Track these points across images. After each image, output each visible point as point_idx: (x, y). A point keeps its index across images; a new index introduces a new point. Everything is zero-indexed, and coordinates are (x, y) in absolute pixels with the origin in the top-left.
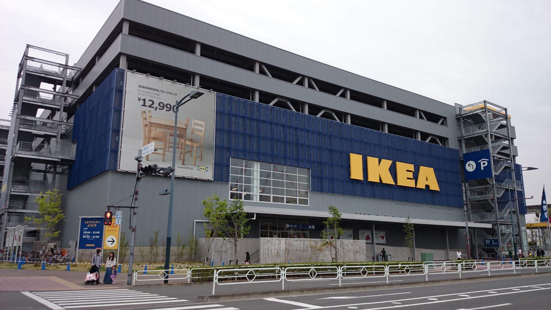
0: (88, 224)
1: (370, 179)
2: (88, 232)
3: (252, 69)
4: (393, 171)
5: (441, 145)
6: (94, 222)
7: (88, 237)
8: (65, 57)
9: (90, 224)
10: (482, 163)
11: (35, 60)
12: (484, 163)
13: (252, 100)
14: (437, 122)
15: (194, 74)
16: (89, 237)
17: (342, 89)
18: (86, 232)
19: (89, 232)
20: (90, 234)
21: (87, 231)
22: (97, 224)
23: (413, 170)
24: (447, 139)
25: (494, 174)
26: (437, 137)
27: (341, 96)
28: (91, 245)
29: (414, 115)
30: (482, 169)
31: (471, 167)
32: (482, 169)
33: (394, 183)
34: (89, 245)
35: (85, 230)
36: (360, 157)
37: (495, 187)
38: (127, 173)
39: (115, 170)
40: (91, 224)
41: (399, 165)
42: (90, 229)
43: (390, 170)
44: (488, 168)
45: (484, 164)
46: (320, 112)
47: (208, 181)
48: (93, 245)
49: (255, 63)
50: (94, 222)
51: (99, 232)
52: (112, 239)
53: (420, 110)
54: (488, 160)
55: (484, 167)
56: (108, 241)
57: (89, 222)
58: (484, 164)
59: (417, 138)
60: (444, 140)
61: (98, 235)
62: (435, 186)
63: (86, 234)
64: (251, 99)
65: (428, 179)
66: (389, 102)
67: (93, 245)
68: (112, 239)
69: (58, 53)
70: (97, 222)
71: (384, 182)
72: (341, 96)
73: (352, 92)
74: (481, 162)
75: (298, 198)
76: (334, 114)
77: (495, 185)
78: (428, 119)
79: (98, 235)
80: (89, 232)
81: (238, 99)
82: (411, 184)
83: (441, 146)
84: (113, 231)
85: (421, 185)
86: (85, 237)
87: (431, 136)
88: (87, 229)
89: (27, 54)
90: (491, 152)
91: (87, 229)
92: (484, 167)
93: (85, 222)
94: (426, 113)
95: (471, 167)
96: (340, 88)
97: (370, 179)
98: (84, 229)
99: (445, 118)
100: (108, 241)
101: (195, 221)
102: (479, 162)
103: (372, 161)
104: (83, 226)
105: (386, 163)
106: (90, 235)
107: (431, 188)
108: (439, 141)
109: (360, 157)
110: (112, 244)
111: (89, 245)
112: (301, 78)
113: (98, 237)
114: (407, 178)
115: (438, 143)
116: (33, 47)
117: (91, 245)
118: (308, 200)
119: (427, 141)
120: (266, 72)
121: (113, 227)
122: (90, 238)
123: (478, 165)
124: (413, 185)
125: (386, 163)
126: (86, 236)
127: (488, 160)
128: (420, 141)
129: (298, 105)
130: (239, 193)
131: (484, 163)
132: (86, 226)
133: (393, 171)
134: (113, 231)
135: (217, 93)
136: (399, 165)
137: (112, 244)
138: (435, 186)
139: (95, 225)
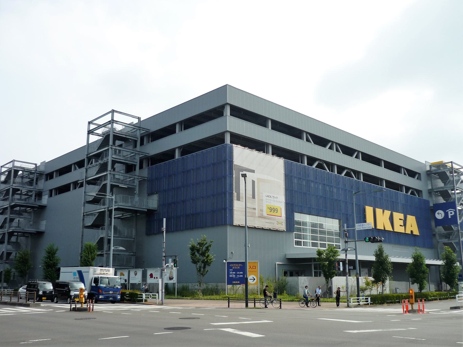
0: (233, 266)
1: (378, 227)
2: (233, 273)
3: (265, 125)
4: (391, 219)
5: (328, 171)
6: (237, 265)
7: (233, 276)
8: (138, 120)
9: (234, 267)
10: (449, 212)
11: (118, 123)
12: (451, 213)
13: (301, 163)
14: (324, 146)
15: (268, 144)
16: (235, 276)
17: (330, 143)
18: (231, 273)
19: (235, 273)
20: (235, 274)
21: (232, 272)
22: (240, 266)
23: (403, 218)
24: (421, 191)
25: (459, 222)
26: (415, 190)
27: (356, 157)
28: (237, 282)
29: (301, 138)
30: (450, 217)
31: (440, 215)
32: (450, 217)
33: (393, 231)
34: (235, 282)
35: (231, 271)
36: (371, 208)
37: (460, 233)
38: (239, 226)
39: (232, 225)
40: (235, 266)
41: (395, 214)
42: (235, 270)
43: (389, 219)
44: (455, 217)
45: (451, 213)
46: (315, 163)
47: (283, 231)
48: (239, 282)
49: (402, 168)
50: (237, 265)
51: (242, 273)
52: (253, 277)
53: (307, 133)
54: (454, 210)
55: (451, 216)
56: (250, 279)
57: (233, 265)
58: (451, 213)
59: (359, 179)
60: (419, 192)
61: (241, 274)
62: (416, 232)
63: (232, 274)
64: (300, 162)
65: (412, 226)
66: (385, 162)
67: (239, 282)
68: (253, 277)
69: (133, 117)
70: (240, 265)
71: (386, 229)
72: (356, 157)
73: (363, 153)
74: (449, 212)
75: (319, 242)
76: (325, 165)
77: (460, 231)
78: (344, 153)
79: (241, 274)
80: (235, 273)
81: (287, 161)
82: (401, 230)
83: (328, 172)
84: (253, 271)
85: (408, 232)
86: (231, 276)
87: (346, 169)
88: (232, 270)
89: (113, 119)
90: (457, 204)
91: (232, 270)
92: (451, 216)
93: (231, 265)
94: (313, 136)
95: (440, 215)
96: (329, 141)
97: (378, 227)
98: (230, 270)
99: (419, 174)
100: (250, 279)
101: (277, 263)
102: (447, 211)
103: (379, 211)
104: (229, 268)
105: (388, 213)
106: (235, 274)
107: (414, 233)
108: (416, 193)
109: (371, 208)
110: (253, 281)
111: (235, 282)
112: (331, 143)
113: (242, 276)
114: (399, 225)
115: (325, 169)
116: (117, 112)
117: (237, 282)
118: (341, 245)
119: (343, 174)
120: (354, 155)
121: (253, 269)
122: (235, 277)
123: (446, 214)
124: (403, 232)
125: (388, 213)
126: (232, 275)
127: (454, 210)
128: (336, 174)
129: (330, 165)
130: (307, 240)
131: (451, 213)
132: (231, 268)
133: (391, 219)
134: (253, 271)
135: (284, 160)
136: (395, 214)
137: (253, 281)
138: (416, 232)
139: (239, 267)
